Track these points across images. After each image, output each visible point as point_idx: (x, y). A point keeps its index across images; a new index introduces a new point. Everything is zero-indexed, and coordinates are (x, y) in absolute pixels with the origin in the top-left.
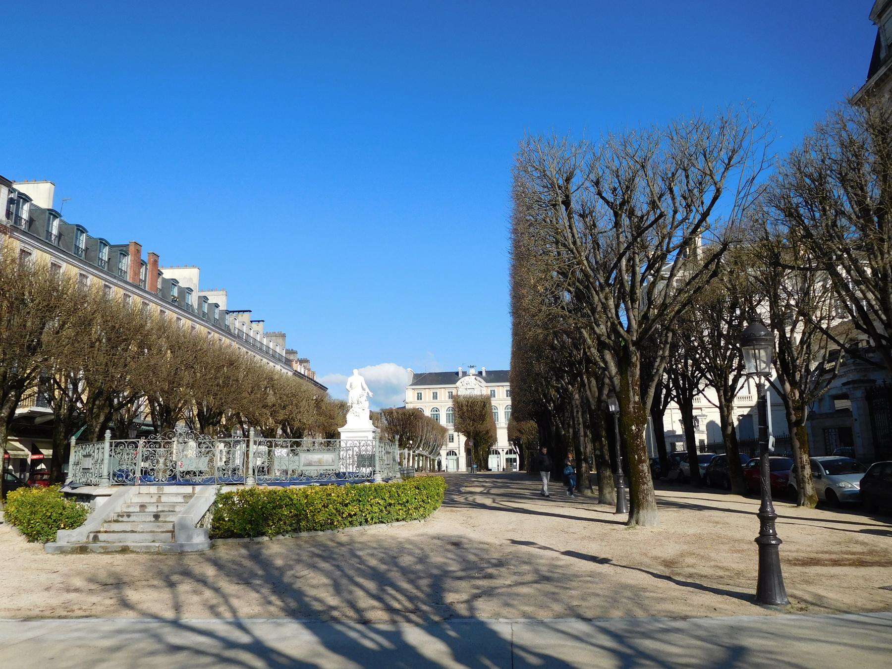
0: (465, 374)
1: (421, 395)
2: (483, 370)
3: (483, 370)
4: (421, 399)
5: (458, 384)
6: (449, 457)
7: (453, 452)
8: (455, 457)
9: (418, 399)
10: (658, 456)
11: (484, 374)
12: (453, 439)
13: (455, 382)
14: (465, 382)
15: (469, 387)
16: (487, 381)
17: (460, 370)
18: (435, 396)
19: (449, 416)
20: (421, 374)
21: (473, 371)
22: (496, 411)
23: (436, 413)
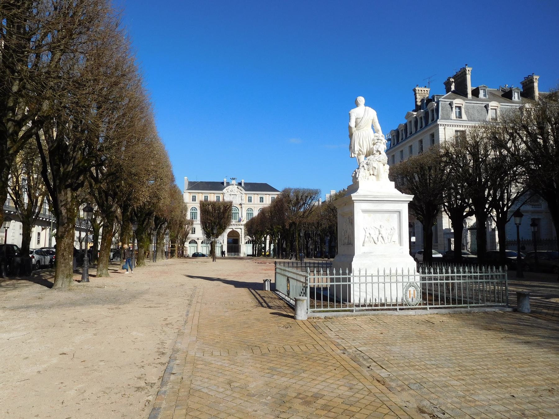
0: (228, 184)
1: (195, 198)
2: (243, 181)
3: (243, 181)
4: (195, 201)
5: (225, 191)
6: (191, 245)
7: (194, 241)
8: (195, 245)
9: (193, 201)
10: (555, 234)
11: (243, 185)
12: (194, 231)
13: (222, 189)
14: (230, 190)
15: (232, 193)
16: (246, 190)
17: (225, 180)
18: (250, 200)
19: (192, 214)
20: (195, 182)
21: (234, 182)
22: (196, 211)
23: (251, 212)
